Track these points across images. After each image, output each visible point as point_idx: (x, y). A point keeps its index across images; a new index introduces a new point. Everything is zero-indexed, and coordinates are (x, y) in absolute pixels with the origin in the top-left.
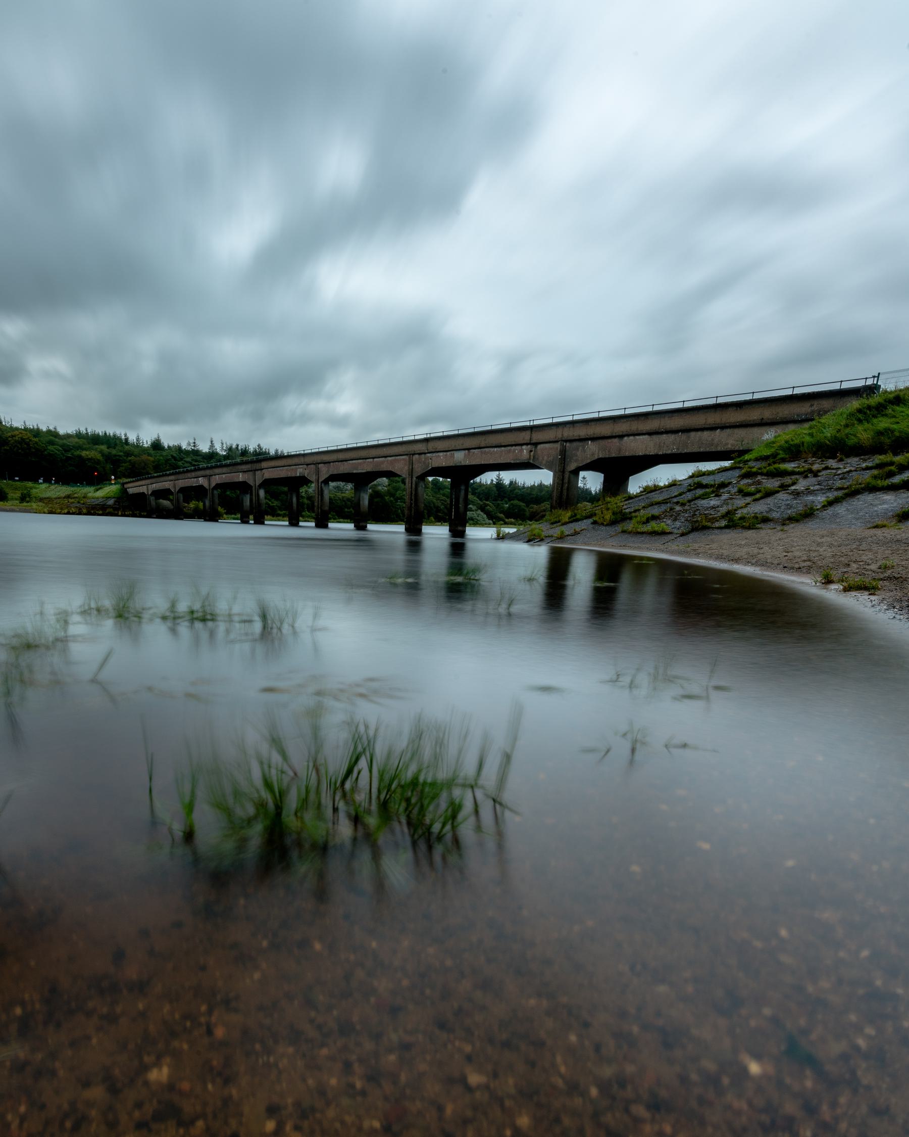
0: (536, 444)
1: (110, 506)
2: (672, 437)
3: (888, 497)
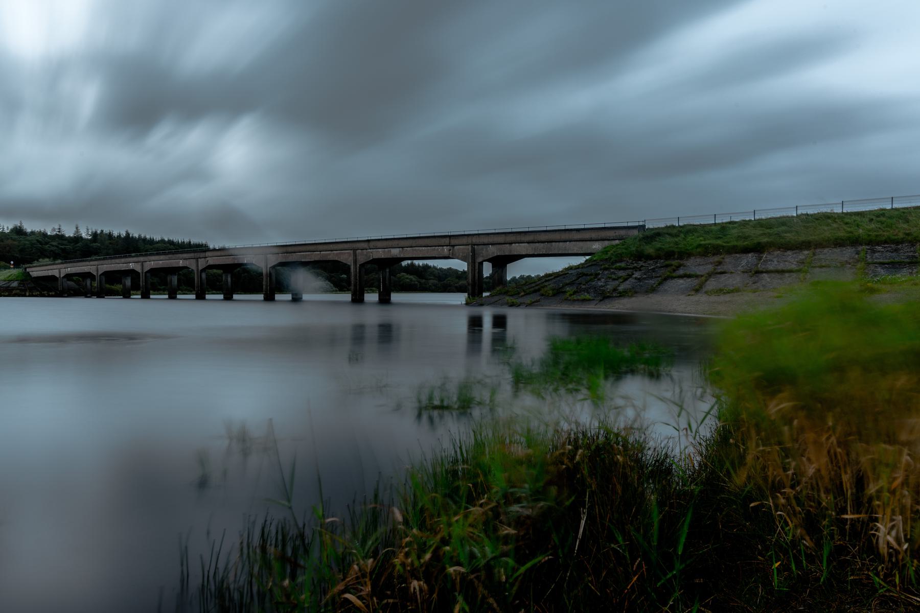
0: (453, 246)
1: (14, 288)
3: (681, 281)
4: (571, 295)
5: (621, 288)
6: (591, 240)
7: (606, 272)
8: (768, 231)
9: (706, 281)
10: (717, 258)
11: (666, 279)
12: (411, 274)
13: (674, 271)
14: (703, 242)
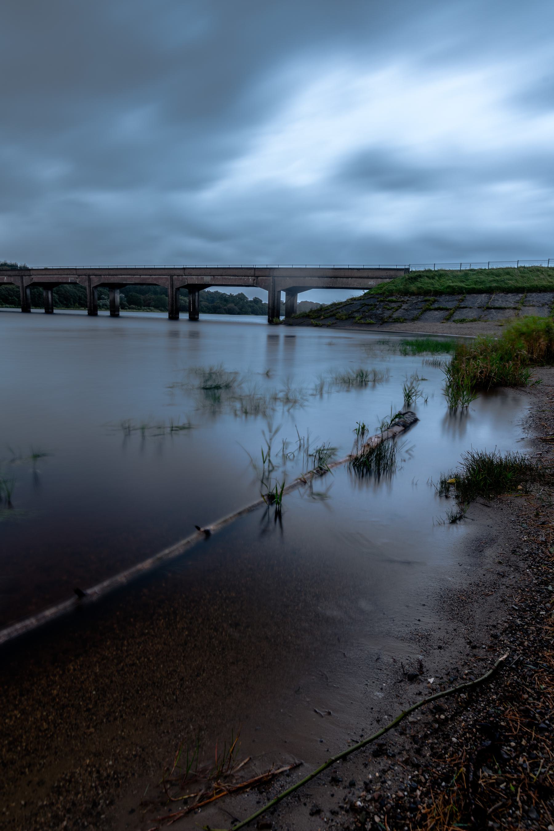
3: (436, 312)
4: (359, 320)
5: (395, 315)
6: (368, 278)
7: (382, 304)
8: (497, 278)
9: (454, 313)
10: (460, 297)
11: (425, 311)
13: (431, 305)
14: (451, 284)
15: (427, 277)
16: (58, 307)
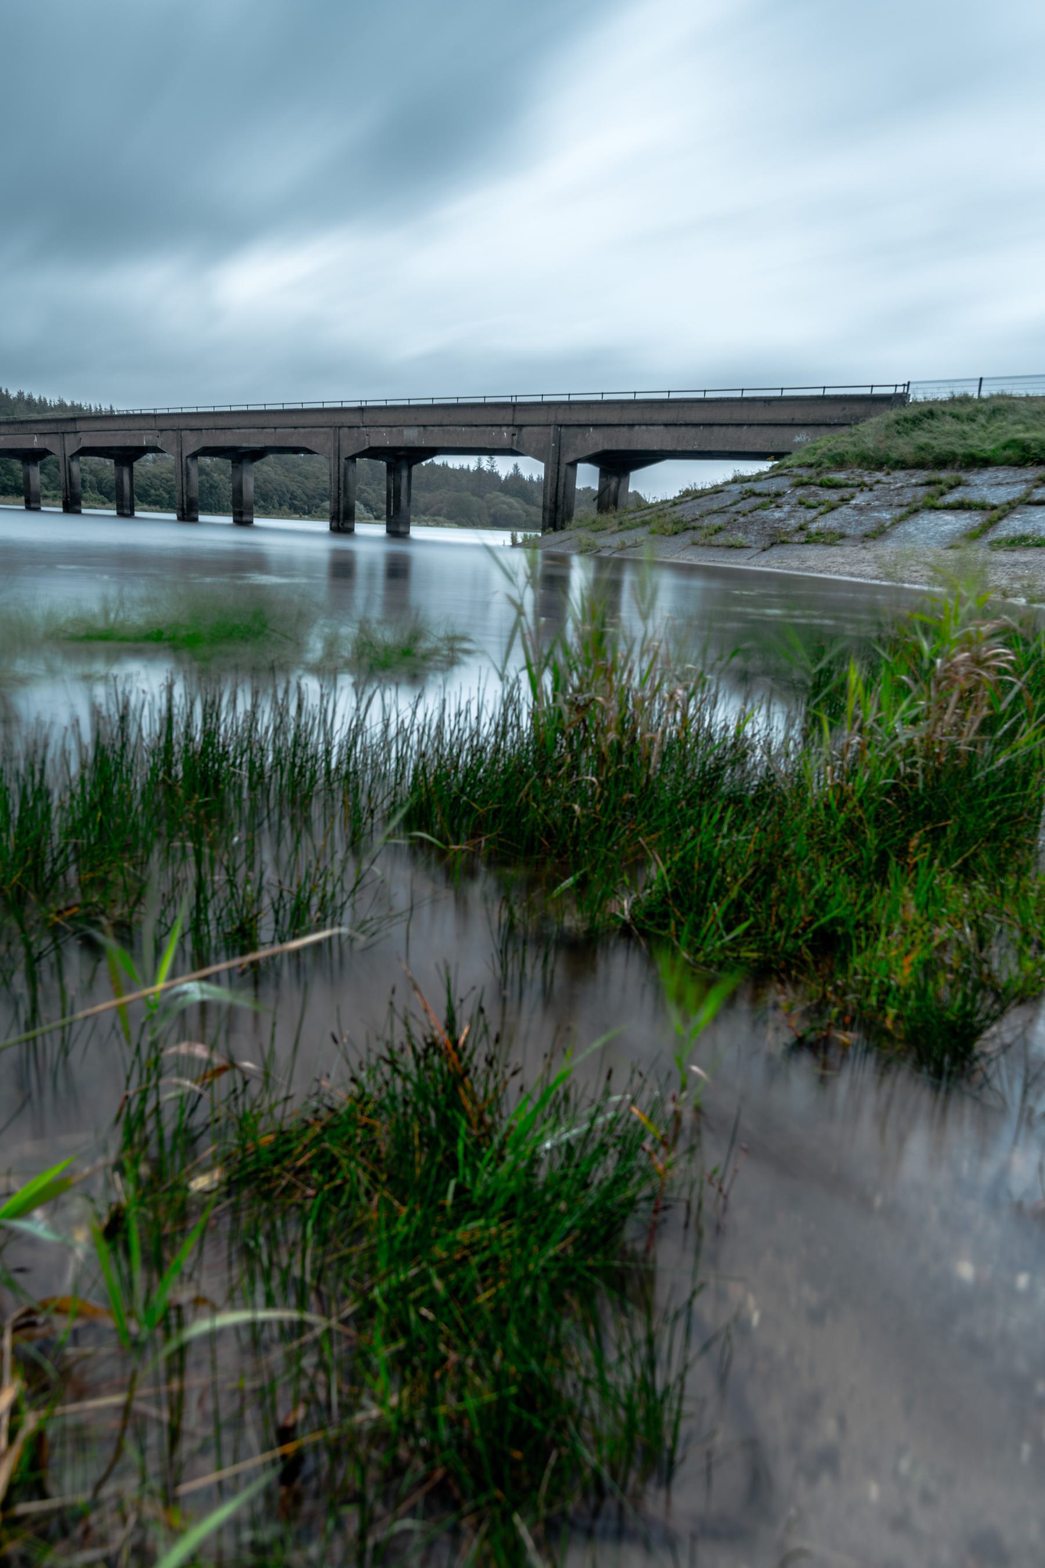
0: (521, 426)
2: (692, 431)
3: (948, 517)
5: (813, 527)
9: (1000, 519)
12: (513, 496)
13: (942, 494)
14: (1021, 435)
15: (956, 417)
16: (267, 513)
